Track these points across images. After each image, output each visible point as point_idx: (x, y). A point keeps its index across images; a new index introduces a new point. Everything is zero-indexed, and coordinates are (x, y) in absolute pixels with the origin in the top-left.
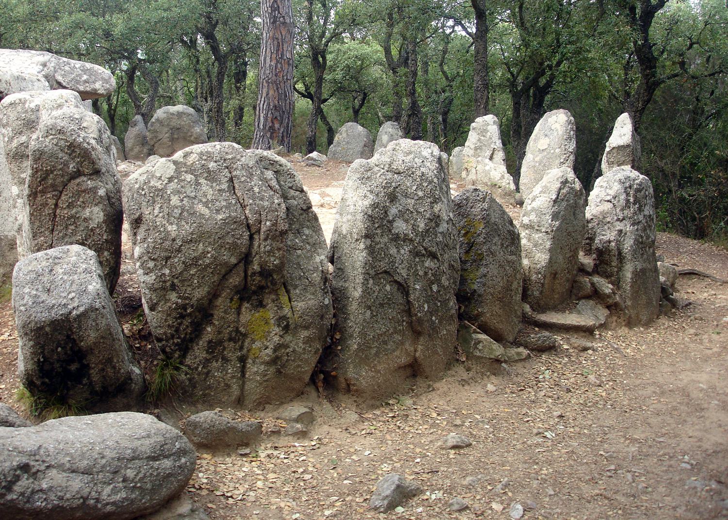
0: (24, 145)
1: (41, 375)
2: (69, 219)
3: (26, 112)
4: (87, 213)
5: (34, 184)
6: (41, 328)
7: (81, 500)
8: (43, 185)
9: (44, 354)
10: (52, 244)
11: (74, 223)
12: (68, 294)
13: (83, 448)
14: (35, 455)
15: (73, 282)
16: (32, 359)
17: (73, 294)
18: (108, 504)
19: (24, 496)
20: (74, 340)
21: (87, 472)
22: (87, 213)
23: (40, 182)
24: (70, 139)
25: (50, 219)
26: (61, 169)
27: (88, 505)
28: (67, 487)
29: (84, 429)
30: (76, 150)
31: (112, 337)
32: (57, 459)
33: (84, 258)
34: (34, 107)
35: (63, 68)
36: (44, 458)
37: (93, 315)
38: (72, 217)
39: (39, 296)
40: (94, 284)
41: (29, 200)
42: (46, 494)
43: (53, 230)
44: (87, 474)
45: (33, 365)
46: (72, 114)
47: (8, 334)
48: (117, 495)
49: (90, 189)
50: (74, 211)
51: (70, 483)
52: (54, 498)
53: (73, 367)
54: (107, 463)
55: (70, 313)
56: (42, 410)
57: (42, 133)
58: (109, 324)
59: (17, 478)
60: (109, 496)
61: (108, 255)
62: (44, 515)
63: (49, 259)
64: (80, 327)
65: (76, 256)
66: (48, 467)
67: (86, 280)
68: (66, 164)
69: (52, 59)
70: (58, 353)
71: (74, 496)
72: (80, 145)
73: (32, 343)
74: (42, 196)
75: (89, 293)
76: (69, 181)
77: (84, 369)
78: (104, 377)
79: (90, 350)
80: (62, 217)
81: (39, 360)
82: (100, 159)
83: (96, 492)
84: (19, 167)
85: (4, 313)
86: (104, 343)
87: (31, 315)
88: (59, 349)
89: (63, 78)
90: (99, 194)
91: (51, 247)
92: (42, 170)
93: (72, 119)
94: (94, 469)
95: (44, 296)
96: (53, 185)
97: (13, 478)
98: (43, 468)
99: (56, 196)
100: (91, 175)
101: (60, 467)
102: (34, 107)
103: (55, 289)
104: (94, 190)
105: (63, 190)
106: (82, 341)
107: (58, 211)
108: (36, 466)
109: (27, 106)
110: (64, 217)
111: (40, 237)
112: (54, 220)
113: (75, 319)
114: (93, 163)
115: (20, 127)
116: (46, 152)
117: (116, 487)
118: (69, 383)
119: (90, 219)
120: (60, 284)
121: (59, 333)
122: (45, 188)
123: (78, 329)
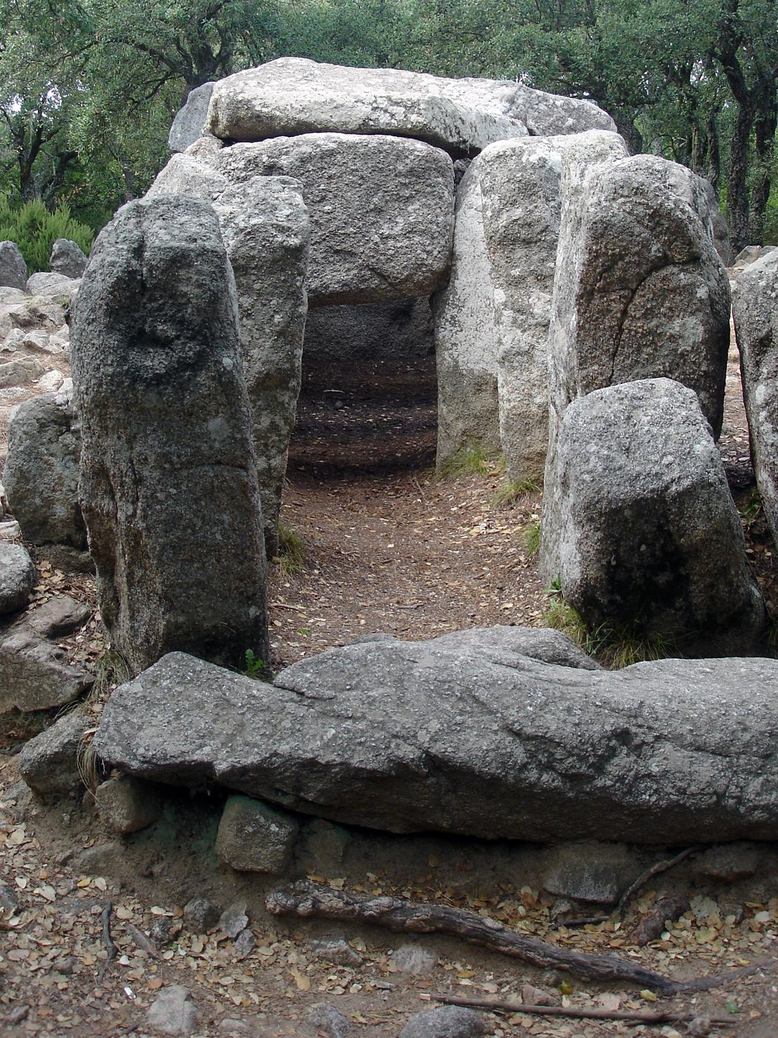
0: (519, 222)
1: (610, 587)
2: (644, 336)
3: (524, 169)
4: (676, 326)
5: (589, 277)
6: (618, 511)
7: (715, 798)
8: (605, 279)
9: (619, 554)
10: (611, 377)
11: (653, 342)
12: (662, 458)
13: (711, 711)
14: (636, 717)
15: (668, 438)
16: (599, 561)
17: (670, 458)
18: (755, 808)
19: (623, 783)
20: (670, 534)
21: (720, 751)
22: (676, 326)
23: (600, 274)
24: (654, 204)
25: (611, 336)
26: (636, 253)
27: (726, 806)
28: (691, 774)
29: (702, 680)
30: (663, 221)
31: (732, 532)
32: (671, 725)
33: (681, 399)
34: (536, 162)
35: (536, 107)
36: (651, 723)
37: (704, 494)
38: (650, 332)
39: (614, 459)
40: (704, 442)
41: (580, 304)
42: (657, 783)
43: (614, 355)
44: (720, 755)
45: (599, 570)
46: (650, 164)
47: (485, 525)
48: (771, 794)
49: (684, 287)
50: (653, 323)
51: (695, 767)
52: (671, 791)
53: (662, 579)
54: (753, 739)
55: (667, 488)
56: (603, 647)
57: (606, 194)
58: (728, 510)
59: (613, 752)
60: (758, 794)
61: (705, 398)
62: (652, 817)
63: (622, 399)
64: (681, 513)
65: (667, 396)
66: (657, 738)
67: (689, 435)
68: (646, 246)
69: (519, 93)
70: (641, 555)
71: (703, 789)
72: (669, 213)
73: (599, 535)
74: (602, 297)
75: (697, 458)
76: (649, 273)
77: (681, 582)
78: (712, 598)
79: (695, 552)
80: (633, 333)
81: (609, 562)
82: (700, 238)
83: (737, 787)
84: (509, 260)
85: (469, 492)
86: (717, 541)
87: (601, 489)
88: (643, 548)
89: (536, 122)
90: (698, 295)
91: (609, 382)
92: (606, 254)
93: (650, 171)
94: (732, 748)
95: (621, 460)
96: (622, 280)
97: (606, 751)
98: (650, 739)
99: (625, 297)
100: (684, 263)
101: (677, 739)
102: (536, 162)
103: (639, 448)
104: (690, 289)
105: (637, 288)
106: (682, 536)
107: (627, 323)
108: (641, 735)
109: (524, 159)
110: (637, 332)
111: (592, 365)
112: (618, 338)
113: (674, 499)
114: (690, 243)
115: (513, 193)
116: (615, 225)
117: (768, 781)
118: (653, 604)
119: (681, 337)
120: (646, 441)
121: (646, 522)
122: (608, 283)
123: (677, 515)
